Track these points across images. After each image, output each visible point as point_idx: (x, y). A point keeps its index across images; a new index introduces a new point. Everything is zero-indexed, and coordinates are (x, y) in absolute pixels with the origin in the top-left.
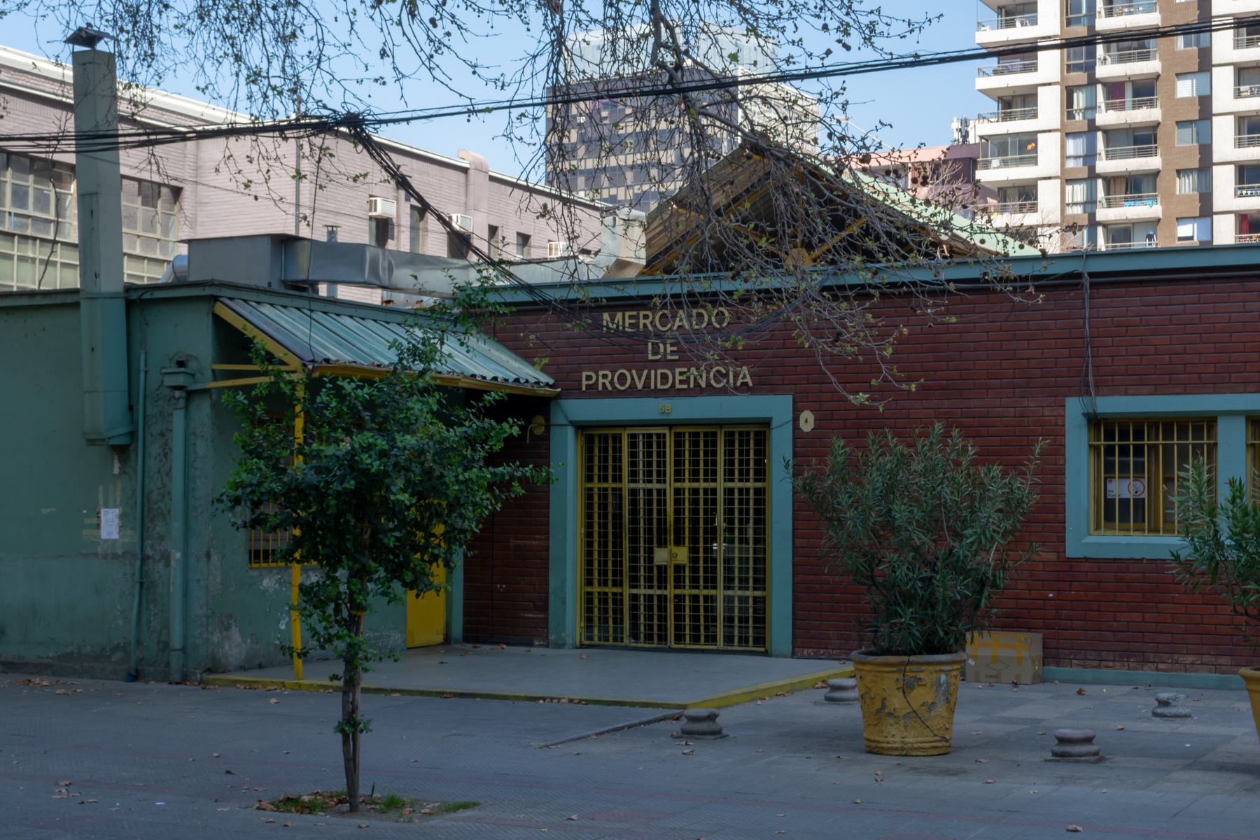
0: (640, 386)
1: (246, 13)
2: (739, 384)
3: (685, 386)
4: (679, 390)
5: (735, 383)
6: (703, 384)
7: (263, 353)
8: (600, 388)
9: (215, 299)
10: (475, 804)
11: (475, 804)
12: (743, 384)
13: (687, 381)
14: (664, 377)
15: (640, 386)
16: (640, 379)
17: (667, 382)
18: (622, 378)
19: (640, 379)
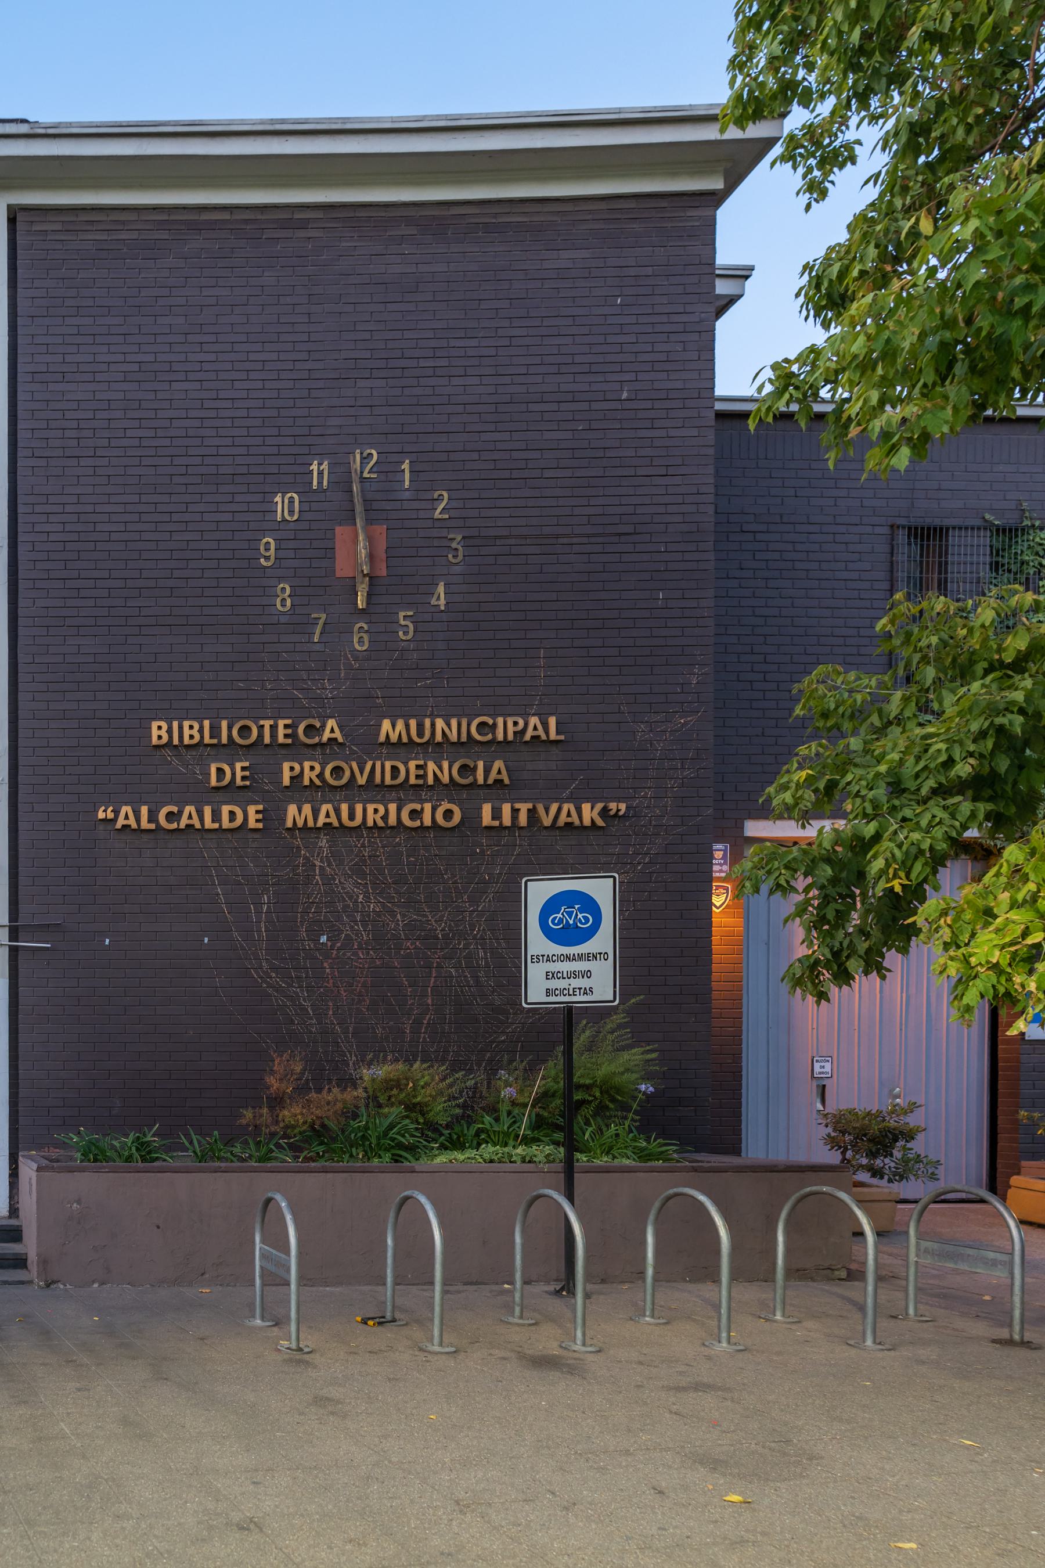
0: (362, 780)
1: (731, 1458)
2: (490, 781)
3: (421, 782)
4: (240, 787)
5: (486, 778)
6: (446, 779)
7: (789, 109)
8: (306, 782)
9: (288, 1348)
10: (994, 1341)
11: (994, 1341)
12: (496, 781)
13: (424, 777)
14: (395, 770)
15: (362, 780)
16: (362, 773)
17: (341, 778)
18: (337, 771)
19: (362, 773)
